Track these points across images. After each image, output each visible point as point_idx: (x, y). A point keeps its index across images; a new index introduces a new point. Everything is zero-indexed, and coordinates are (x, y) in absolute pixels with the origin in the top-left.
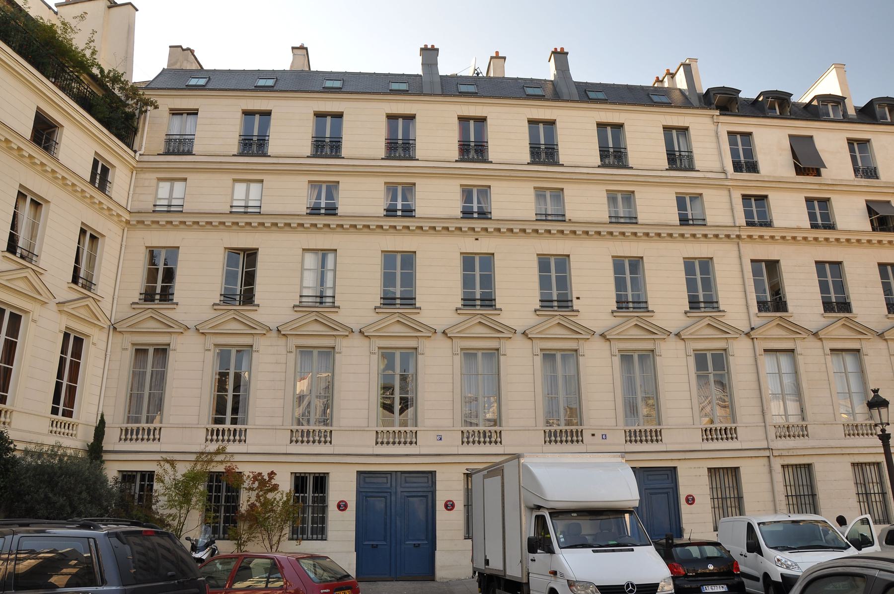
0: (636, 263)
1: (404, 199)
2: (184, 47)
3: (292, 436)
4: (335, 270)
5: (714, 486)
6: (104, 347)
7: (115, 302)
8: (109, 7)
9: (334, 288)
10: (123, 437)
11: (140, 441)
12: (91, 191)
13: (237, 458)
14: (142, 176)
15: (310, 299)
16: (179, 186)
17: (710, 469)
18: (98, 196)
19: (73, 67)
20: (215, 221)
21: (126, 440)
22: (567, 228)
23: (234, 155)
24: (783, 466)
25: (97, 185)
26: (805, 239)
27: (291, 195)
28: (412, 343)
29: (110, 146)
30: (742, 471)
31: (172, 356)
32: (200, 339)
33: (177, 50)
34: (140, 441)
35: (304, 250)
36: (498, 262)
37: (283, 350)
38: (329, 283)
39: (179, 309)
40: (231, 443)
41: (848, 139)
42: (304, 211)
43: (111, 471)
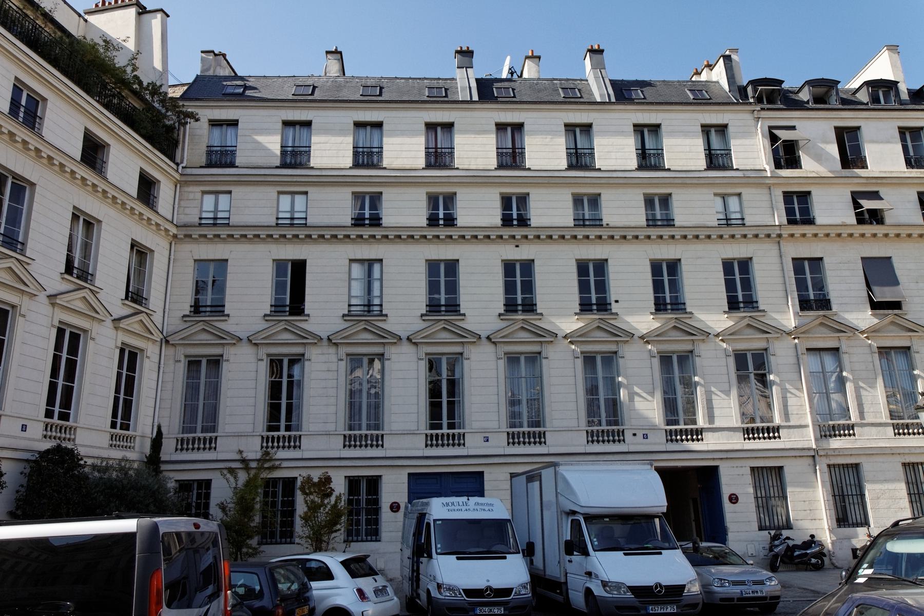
0: (674, 266)
1: (446, 208)
3: (345, 441)
4: (381, 280)
5: (758, 484)
6: (157, 360)
7: (166, 315)
9: (381, 297)
10: (179, 447)
14: (186, 189)
15: (359, 308)
16: (224, 199)
17: (752, 469)
18: (147, 213)
19: (115, 83)
20: (263, 233)
21: (182, 449)
22: (605, 233)
23: (277, 167)
24: (829, 466)
26: (851, 235)
27: (335, 207)
28: (458, 349)
30: (786, 469)
31: (225, 366)
35: (350, 260)
36: (538, 268)
37: (334, 358)
38: (376, 292)
39: (231, 320)
41: (899, 128)
42: (348, 221)
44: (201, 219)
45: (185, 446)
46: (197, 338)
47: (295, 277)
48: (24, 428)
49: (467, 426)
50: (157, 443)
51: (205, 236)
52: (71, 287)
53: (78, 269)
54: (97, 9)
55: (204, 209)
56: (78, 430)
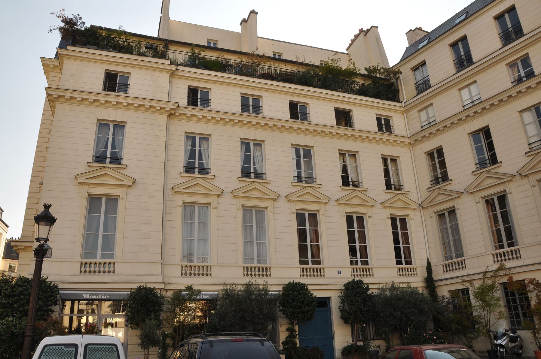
2: (413, 29)
8: (365, 35)
10: (445, 270)
11: (455, 270)
13: (514, 271)
14: (410, 114)
15: (538, 144)
23: (500, 49)
25: (385, 131)
27: (499, 79)
29: (384, 107)
31: (458, 212)
32: (471, 197)
33: (410, 33)
34: (455, 270)
35: (520, 112)
39: (454, 182)
40: (507, 261)
43: (444, 292)
45: (448, 269)
47: (437, 157)
49: (465, 255)
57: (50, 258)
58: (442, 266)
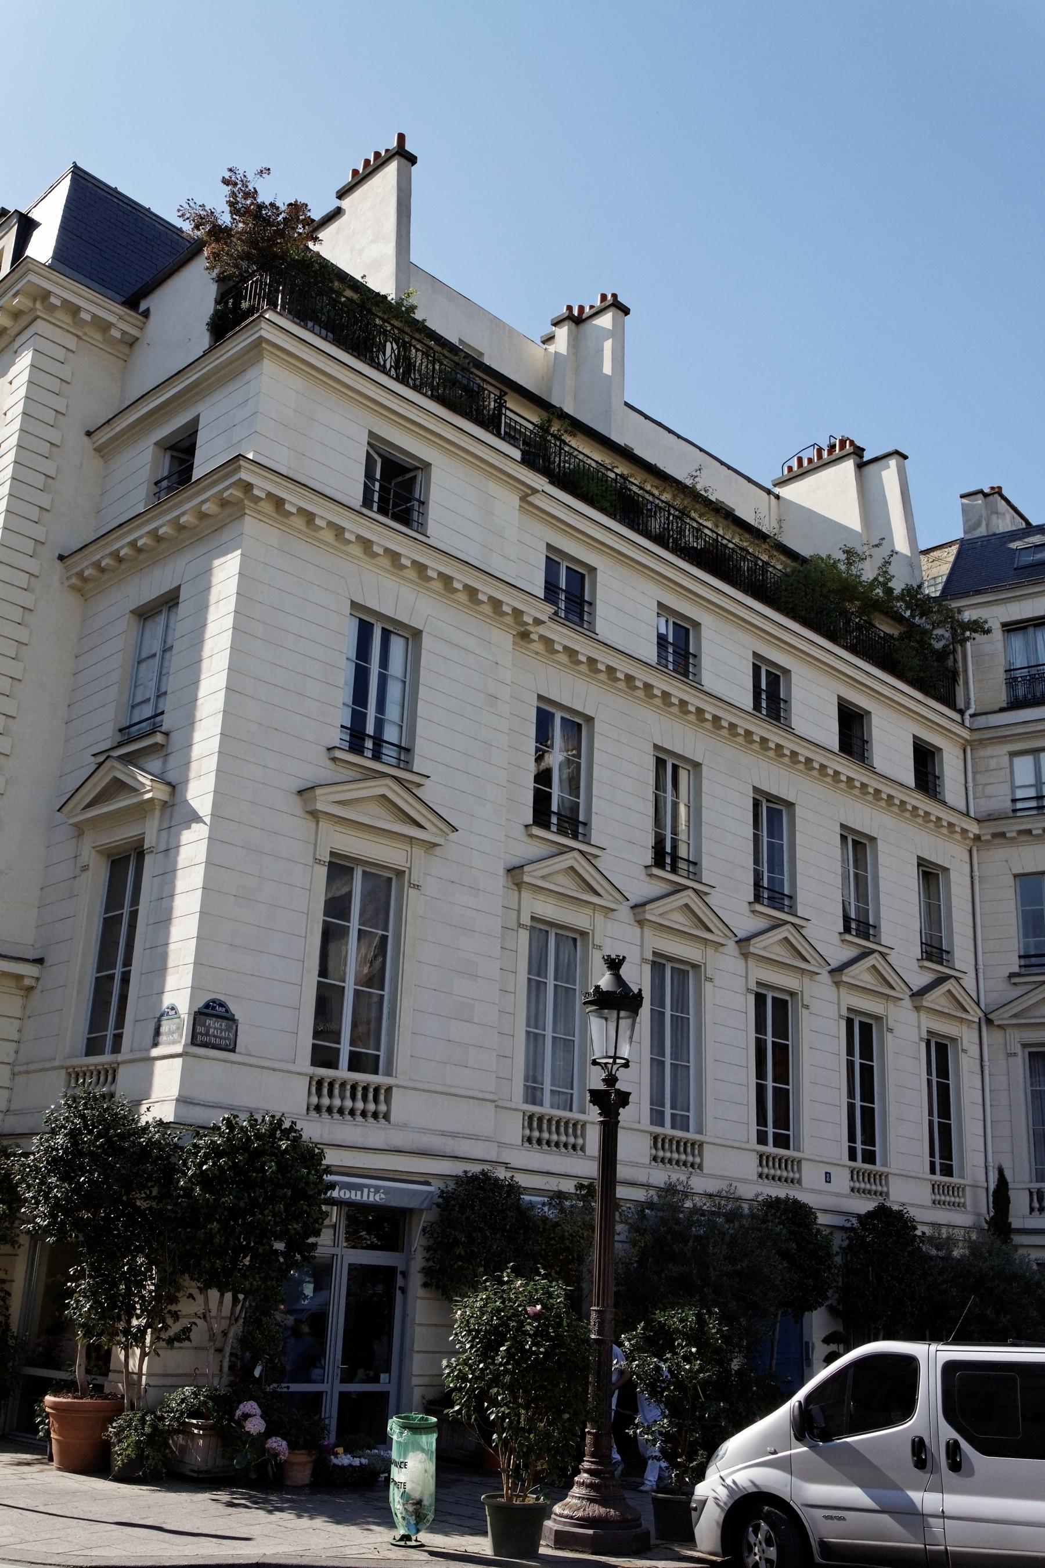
6: (977, 1055)
7: (981, 976)
12: (761, 729)
14: (982, 753)
44: (1014, 801)
46: (1038, 1013)
48: (828, 1178)
50: (1001, 1195)
51: (1029, 832)
52: (665, 888)
53: (772, 891)
54: (792, 475)
55: (1018, 783)
56: (891, 1179)
57: (233, 1050)
58: (1027, 1193)
